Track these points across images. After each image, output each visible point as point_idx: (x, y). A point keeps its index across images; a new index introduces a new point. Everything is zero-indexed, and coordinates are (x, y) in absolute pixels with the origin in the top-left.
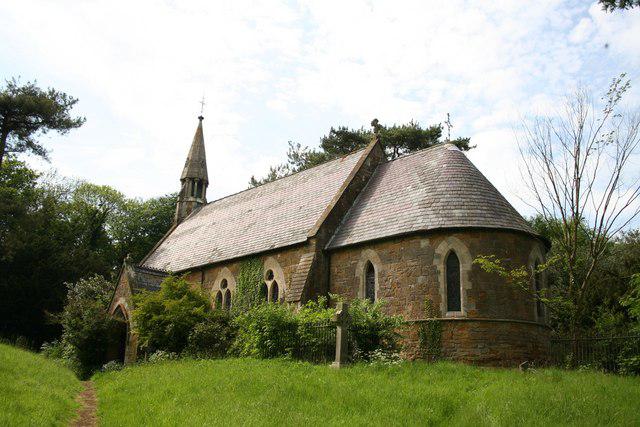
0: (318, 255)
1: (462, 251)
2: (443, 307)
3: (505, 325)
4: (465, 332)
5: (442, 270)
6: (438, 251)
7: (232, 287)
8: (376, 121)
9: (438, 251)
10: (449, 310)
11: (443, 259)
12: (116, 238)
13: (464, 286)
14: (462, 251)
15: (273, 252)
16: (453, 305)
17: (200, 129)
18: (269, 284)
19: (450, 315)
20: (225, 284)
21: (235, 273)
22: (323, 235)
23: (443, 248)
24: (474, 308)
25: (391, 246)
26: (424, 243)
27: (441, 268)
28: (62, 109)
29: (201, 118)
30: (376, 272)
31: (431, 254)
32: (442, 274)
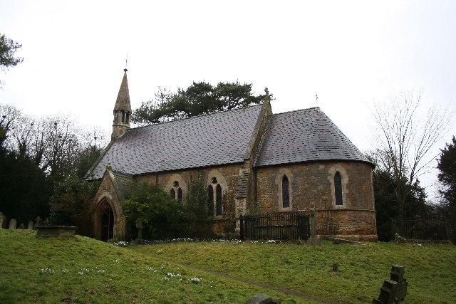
2: (334, 203)
5: (333, 183)
6: (330, 172)
7: (184, 187)
8: (267, 89)
13: (345, 191)
14: (343, 172)
15: (217, 166)
16: (339, 202)
17: (125, 77)
18: (214, 186)
19: (337, 207)
20: (176, 184)
21: (331, 206)
23: (333, 170)
25: (300, 168)
26: (322, 167)
27: (332, 181)
28: (6, 49)
29: (126, 70)
30: (290, 182)
31: (326, 173)
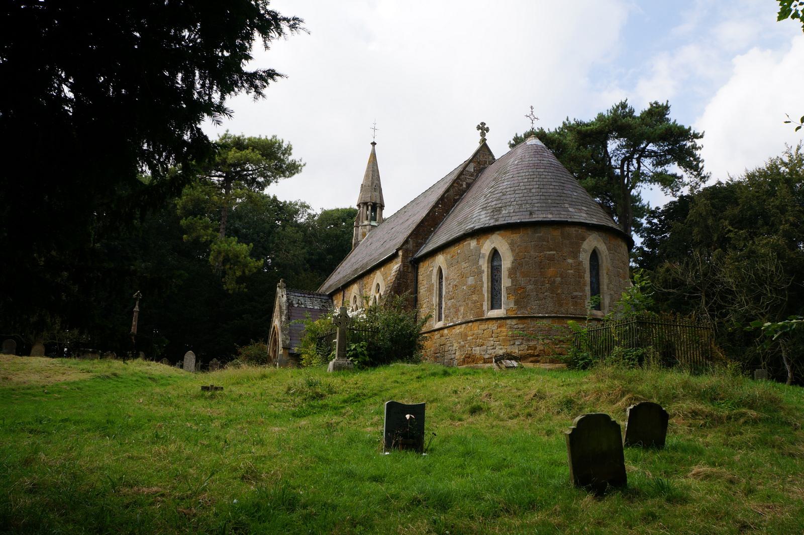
0: (404, 264)
1: (602, 247)
2: (486, 306)
3: (545, 321)
4: (504, 329)
5: (486, 270)
9: (483, 251)
10: (492, 308)
11: (487, 258)
12: (145, 176)
13: (506, 282)
17: (373, 156)
22: (410, 245)
23: (487, 245)
24: (512, 305)
27: (484, 265)
29: (374, 144)
32: (486, 273)
